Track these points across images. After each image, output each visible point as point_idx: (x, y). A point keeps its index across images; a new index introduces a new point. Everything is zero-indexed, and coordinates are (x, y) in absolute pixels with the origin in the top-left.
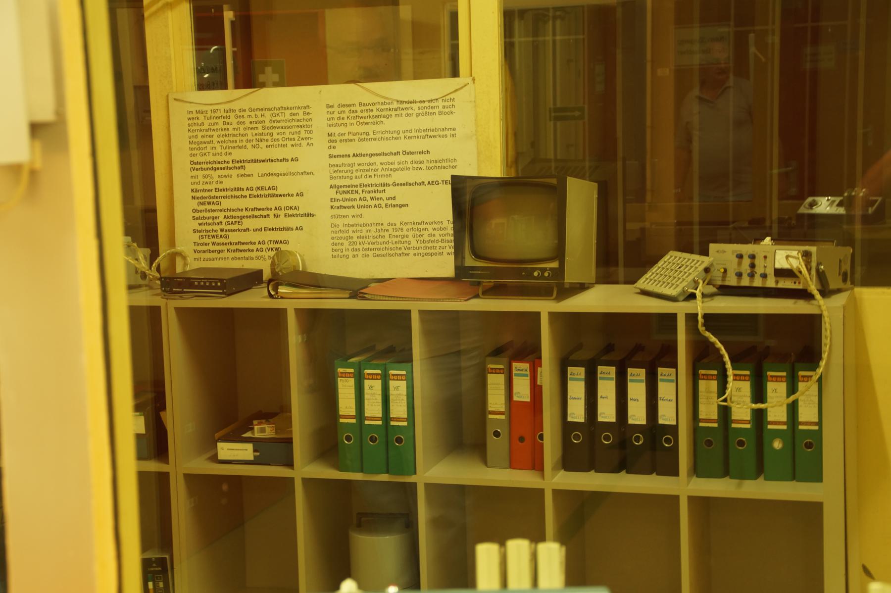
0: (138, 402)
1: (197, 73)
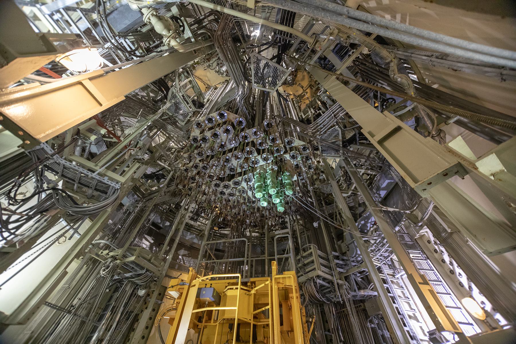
0: (491, 313)
1: (94, 26)
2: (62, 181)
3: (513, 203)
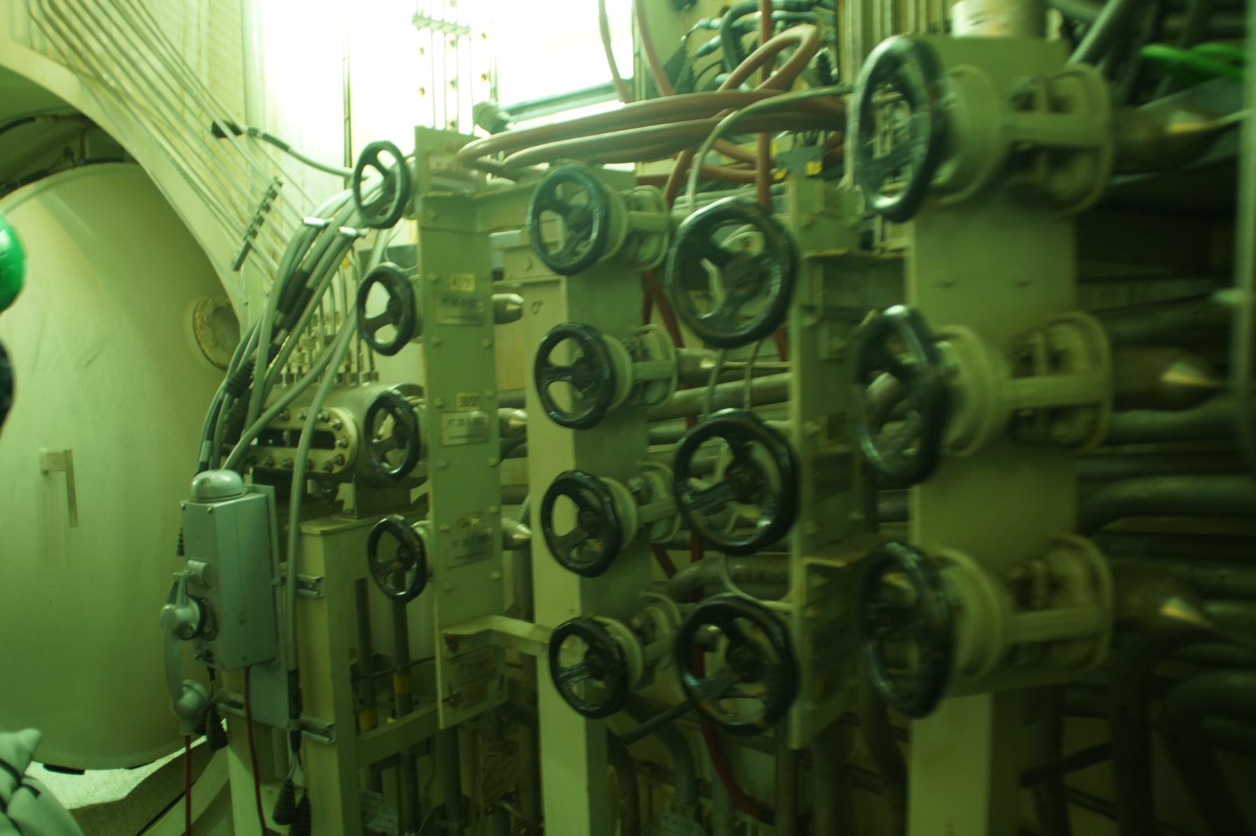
0: (762, 9)
2: (297, 806)
3: (414, 523)
